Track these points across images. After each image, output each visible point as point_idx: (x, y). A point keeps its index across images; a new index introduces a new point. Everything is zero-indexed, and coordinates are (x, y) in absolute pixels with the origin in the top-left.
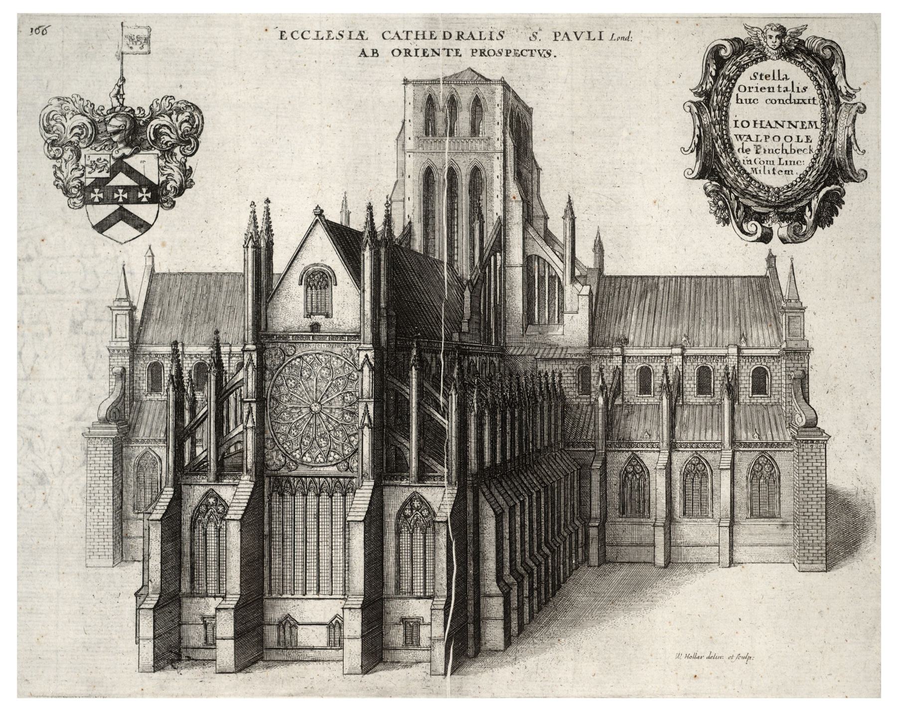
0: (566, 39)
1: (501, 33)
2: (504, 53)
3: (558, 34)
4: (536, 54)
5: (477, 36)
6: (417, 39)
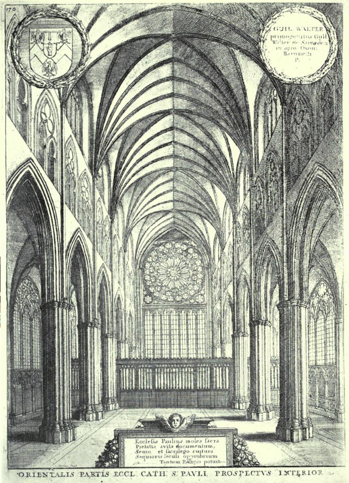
6: (161, 475)
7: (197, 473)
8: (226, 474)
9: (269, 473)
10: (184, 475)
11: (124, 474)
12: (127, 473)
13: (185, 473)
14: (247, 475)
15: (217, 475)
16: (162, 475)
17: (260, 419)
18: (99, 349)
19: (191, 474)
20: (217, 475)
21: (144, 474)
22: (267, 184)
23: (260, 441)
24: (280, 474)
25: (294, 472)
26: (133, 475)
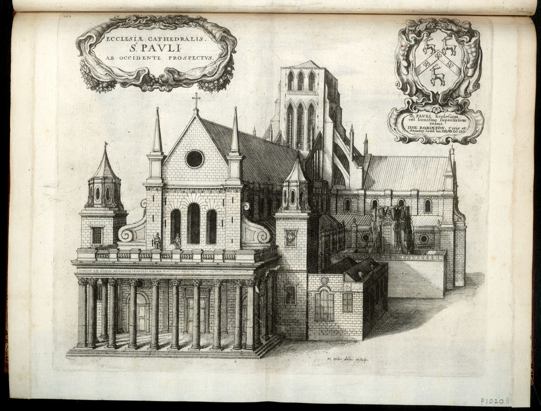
0: (152, 50)
1: (133, 46)
2: (187, 58)
3: (145, 46)
4: (204, 58)
5: (190, 39)
6: (165, 40)
7: (167, 47)
8: (177, 58)
9: (132, 47)
10: (145, 49)
11: (115, 39)
12: (118, 38)
13: (146, 46)
14: (170, 51)
15: (143, 51)
16: (166, 40)
17: (83, 218)
18: (194, 315)
19: (422, 116)
20: (143, 51)
21: (150, 39)
22: (290, 325)
23: (386, 335)
24: (178, 45)
25: (155, 58)
26: (172, 50)
